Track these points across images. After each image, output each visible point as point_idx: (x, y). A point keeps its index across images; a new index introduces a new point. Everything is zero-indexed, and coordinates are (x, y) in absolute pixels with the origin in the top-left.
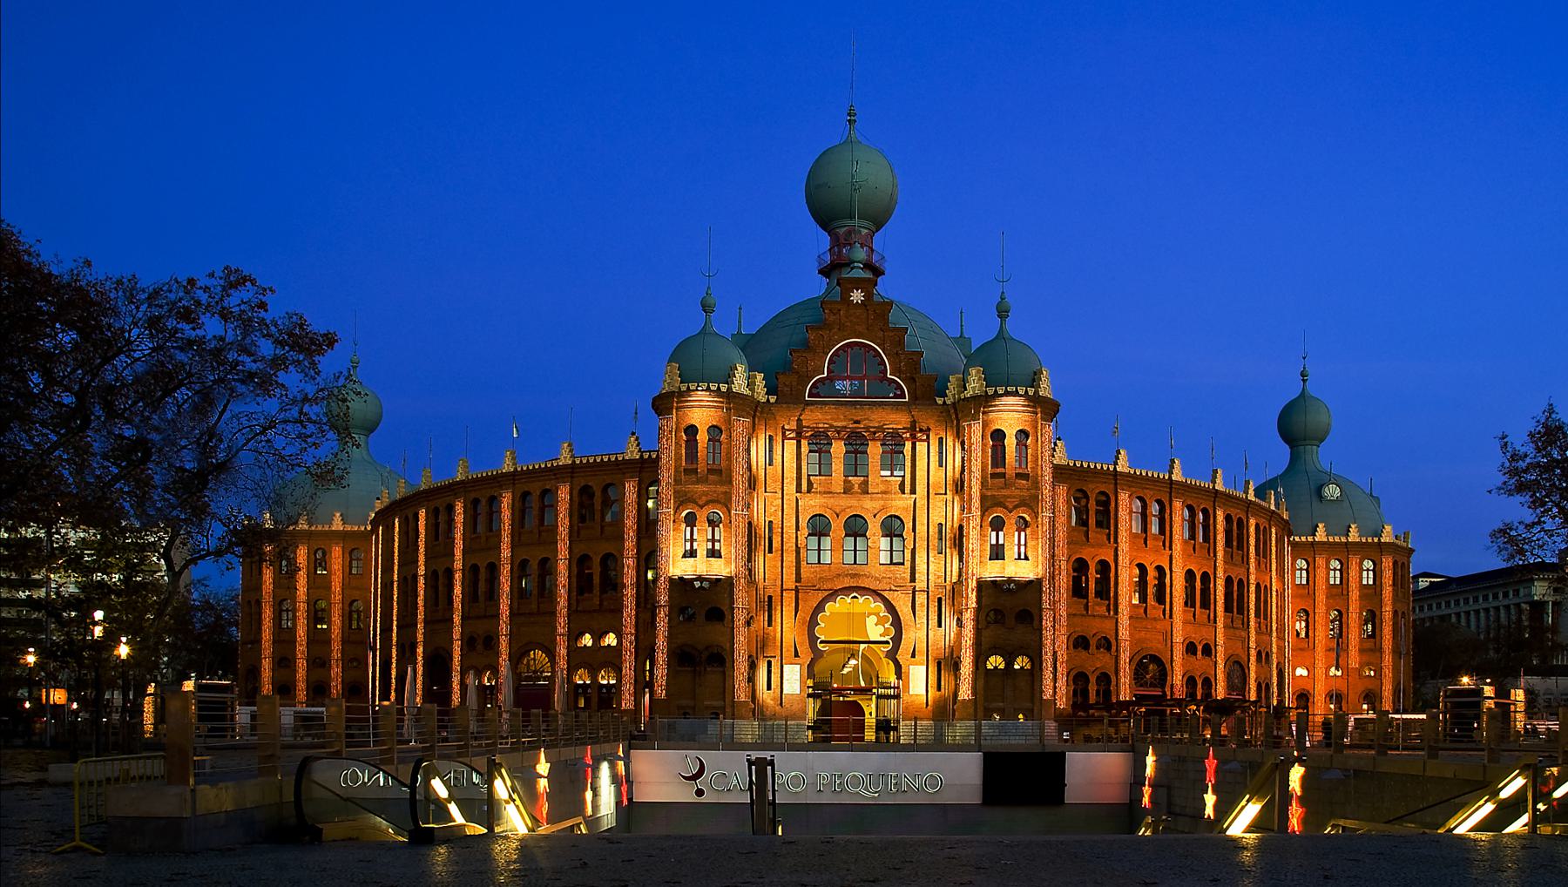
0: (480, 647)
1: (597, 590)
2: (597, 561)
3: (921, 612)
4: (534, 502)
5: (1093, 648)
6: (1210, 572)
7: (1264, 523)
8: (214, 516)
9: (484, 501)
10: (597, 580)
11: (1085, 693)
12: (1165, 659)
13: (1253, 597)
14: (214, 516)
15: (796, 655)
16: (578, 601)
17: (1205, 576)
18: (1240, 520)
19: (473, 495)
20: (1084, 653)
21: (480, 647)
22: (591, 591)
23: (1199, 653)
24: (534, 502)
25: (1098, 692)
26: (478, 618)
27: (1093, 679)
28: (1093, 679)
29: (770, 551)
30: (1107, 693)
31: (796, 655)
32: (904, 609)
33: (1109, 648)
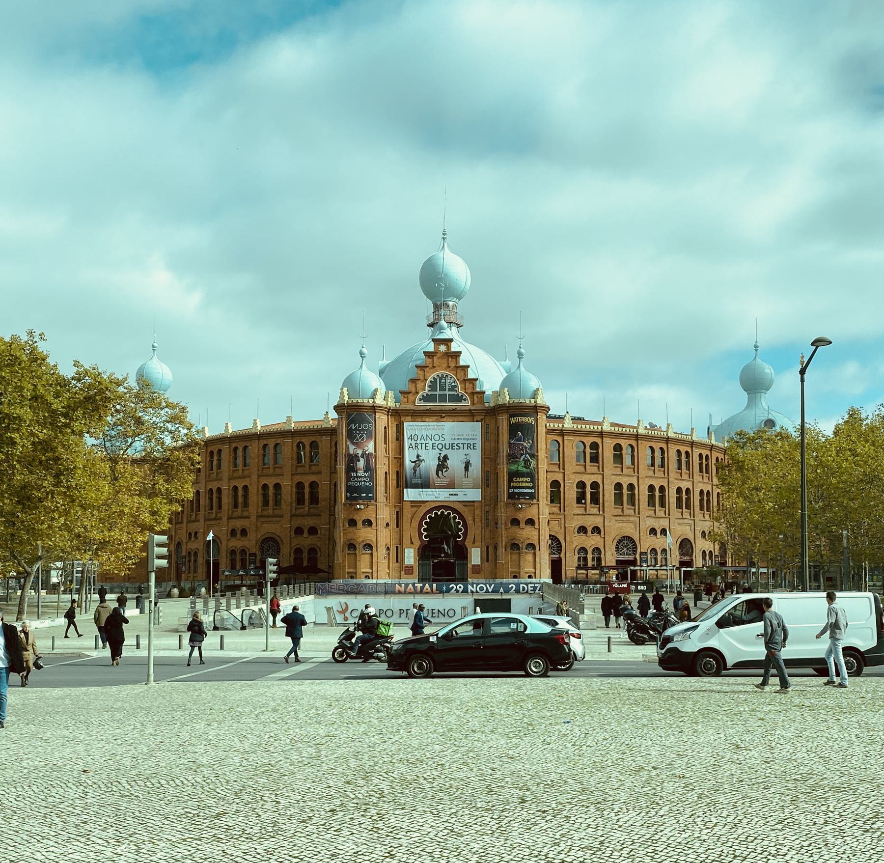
0: (239, 535)
1: (307, 502)
2: (307, 485)
3: (477, 520)
4: (271, 451)
5: (522, 525)
6: (666, 485)
7: (721, 456)
8: (831, 598)
9: (240, 449)
10: (307, 496)
11: (585, 559)
12: (636, 538)
13: (715, 500)
14: (831, 598)
15: (412, 543)
16: (296, 509)
17: (662, 489)
18: (707, 456)
19: (234, 445)
20: (584, 537)
21: (239, 535)
22: (304, 504)
23: (659, 533)
24: (271, 451)
25: (593, 559)
26: (238, 518)
27: (590, 551)
28: (590, 551)
29: (488, 561)
30: (599, 560)
31: (412, 543)
32: (470, 522)
33: (599, 533)
